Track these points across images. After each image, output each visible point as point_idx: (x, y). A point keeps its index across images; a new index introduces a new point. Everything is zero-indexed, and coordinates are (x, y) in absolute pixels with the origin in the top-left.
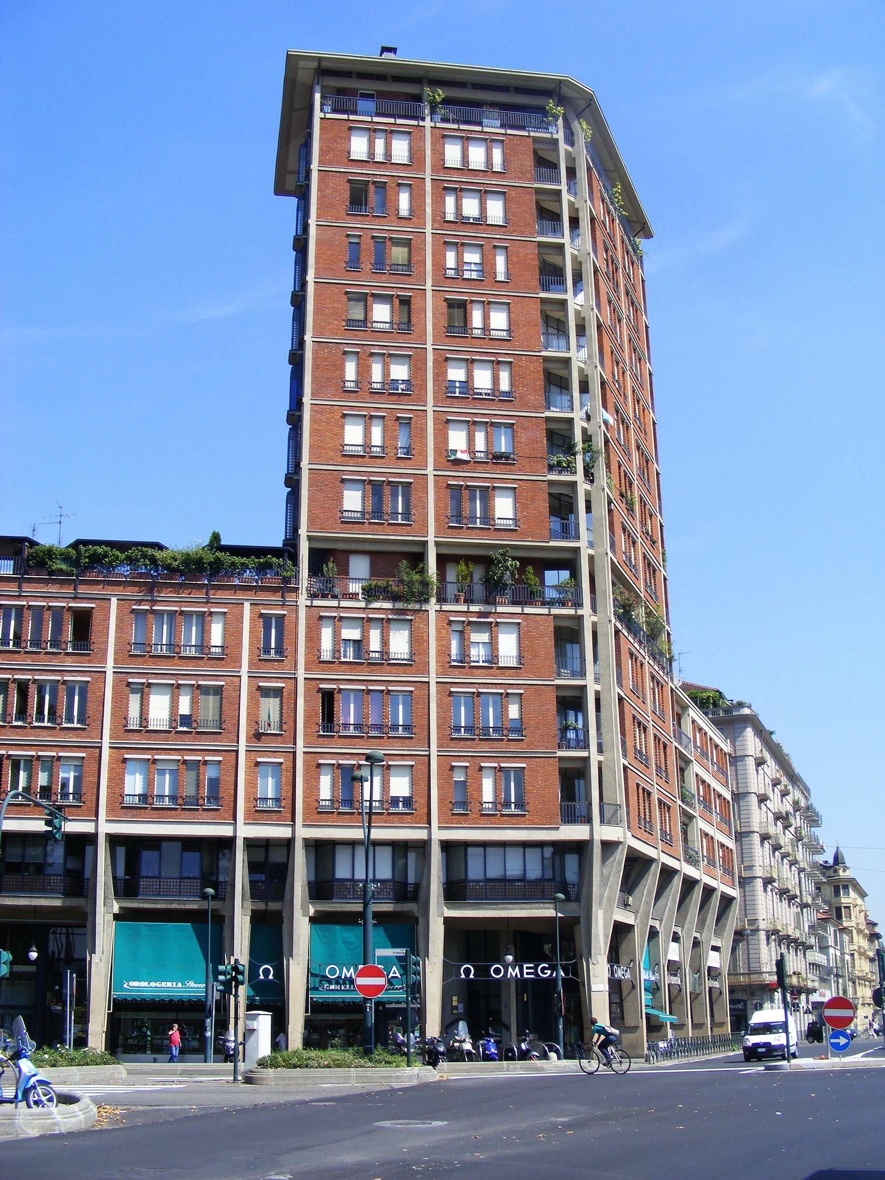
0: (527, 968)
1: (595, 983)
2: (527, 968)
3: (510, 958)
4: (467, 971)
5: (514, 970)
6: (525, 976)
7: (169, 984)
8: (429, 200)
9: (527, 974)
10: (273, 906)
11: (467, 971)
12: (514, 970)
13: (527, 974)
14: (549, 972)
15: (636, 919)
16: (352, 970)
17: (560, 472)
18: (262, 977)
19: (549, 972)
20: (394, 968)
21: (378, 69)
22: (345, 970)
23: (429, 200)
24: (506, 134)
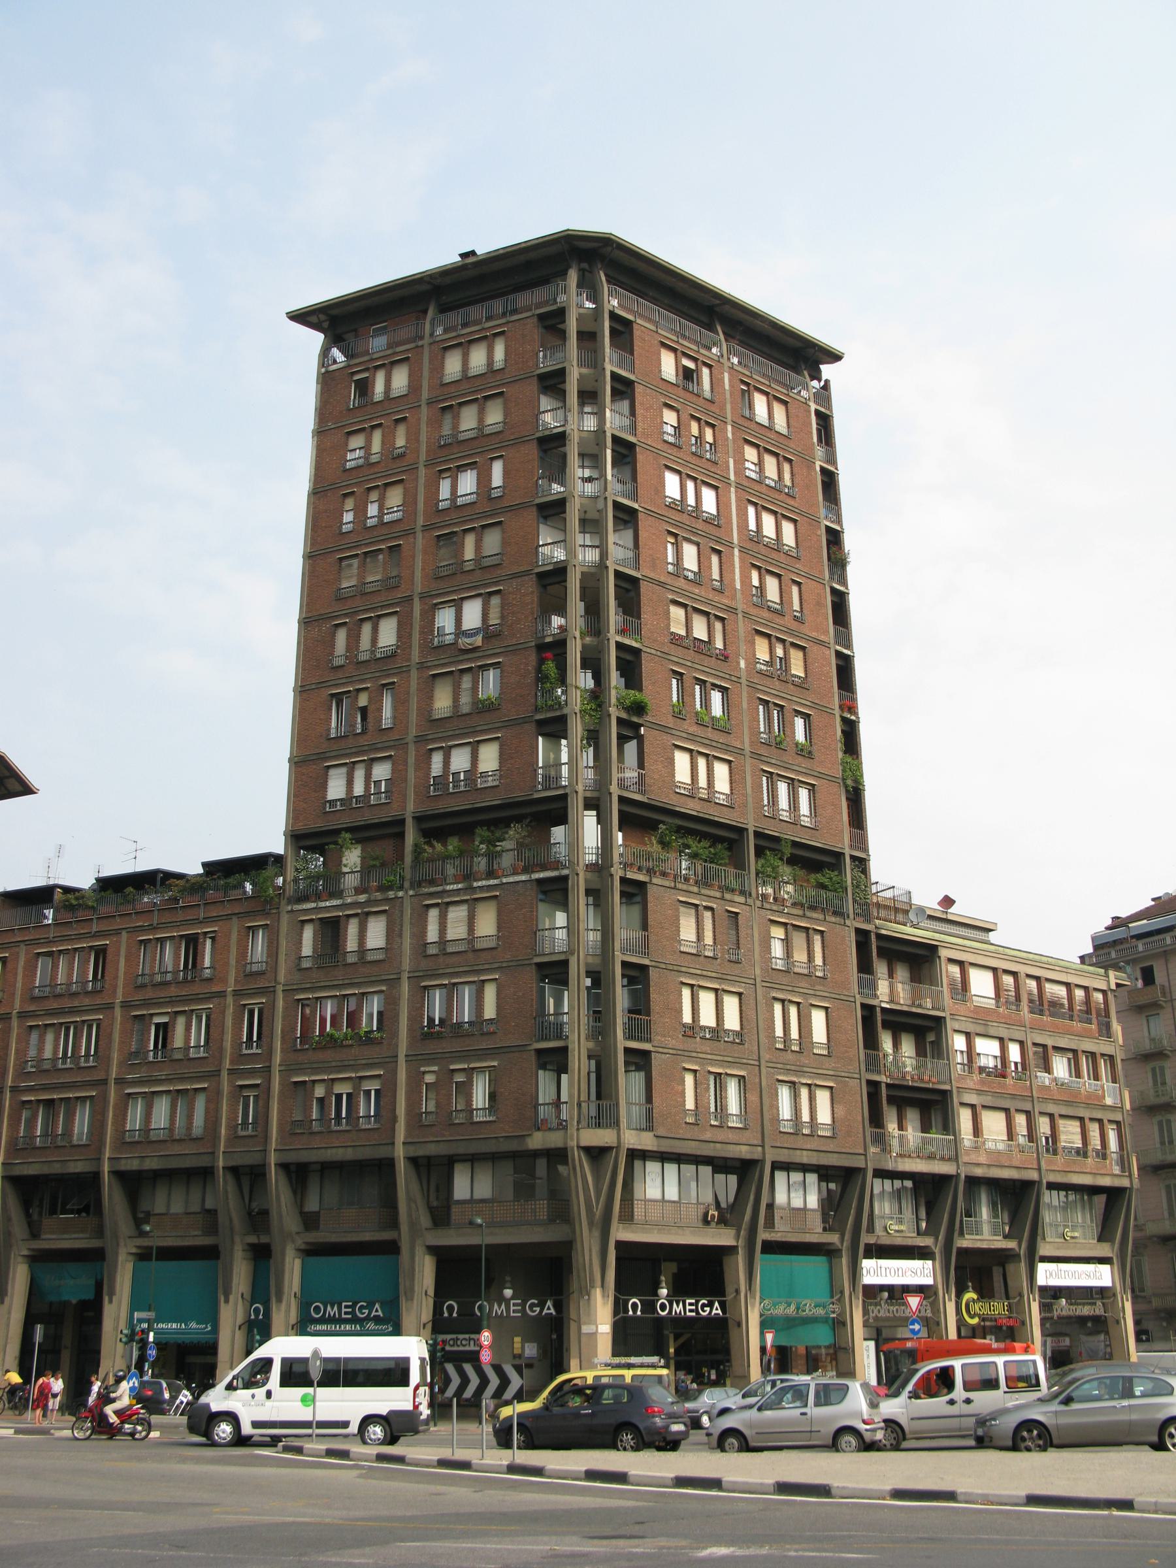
0: (346, 1307)
1: (585, 1323)
2: (346, 1307)
3: (508, 1293)
4: (450, 1308)
5: (500, 1307)
6: (688, 1314)
7: (174, 1326)
8: (737, 571)
9: (346, 1313)
10: (264, 1239)
11: (450, 1308)
12: (500, 1307)
13: (346, 1313)
14: (538, 1309)
15: (737, 1237)
16: (503, 1306)
17: (421, 633)
18: (446, 1315)
19: (538, 1309)
20: (377, 1306)
21: (357, 304)
22: (496, 1306)
23: (737, 571)
24: (508, 322)
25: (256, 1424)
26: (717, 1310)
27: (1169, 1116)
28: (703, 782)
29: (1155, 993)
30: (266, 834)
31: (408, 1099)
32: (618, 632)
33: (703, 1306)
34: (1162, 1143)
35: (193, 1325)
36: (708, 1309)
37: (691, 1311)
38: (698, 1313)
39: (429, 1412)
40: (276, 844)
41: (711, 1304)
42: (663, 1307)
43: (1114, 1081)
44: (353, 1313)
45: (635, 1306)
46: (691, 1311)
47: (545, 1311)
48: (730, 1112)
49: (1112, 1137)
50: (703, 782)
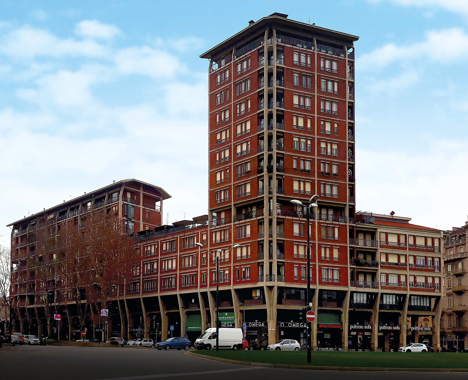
0: (297, 324)
5: (294, 325)
25: (422, 346)
26: (263, 325)
27: (461, 277)
28: (302, 189)
29: (185, 213)
30: (204, 211)
31: (233, 275)
32: (277, 149)
33: (260, 324)
34: (459, 285)
35: (198, 327)
36: (229, 325)
37: (257, 325)
38: (300, 326)
39: (424, 345)
40: (206, 213)
41: (261, 324)
42: (290, 325)
43: (438, 269)
44: (226, 326)
45: (282, 324)
46: (257, 325)
47: (304, 326)
48: (302, 276)
49: (296, 274)
50: (302, 189)
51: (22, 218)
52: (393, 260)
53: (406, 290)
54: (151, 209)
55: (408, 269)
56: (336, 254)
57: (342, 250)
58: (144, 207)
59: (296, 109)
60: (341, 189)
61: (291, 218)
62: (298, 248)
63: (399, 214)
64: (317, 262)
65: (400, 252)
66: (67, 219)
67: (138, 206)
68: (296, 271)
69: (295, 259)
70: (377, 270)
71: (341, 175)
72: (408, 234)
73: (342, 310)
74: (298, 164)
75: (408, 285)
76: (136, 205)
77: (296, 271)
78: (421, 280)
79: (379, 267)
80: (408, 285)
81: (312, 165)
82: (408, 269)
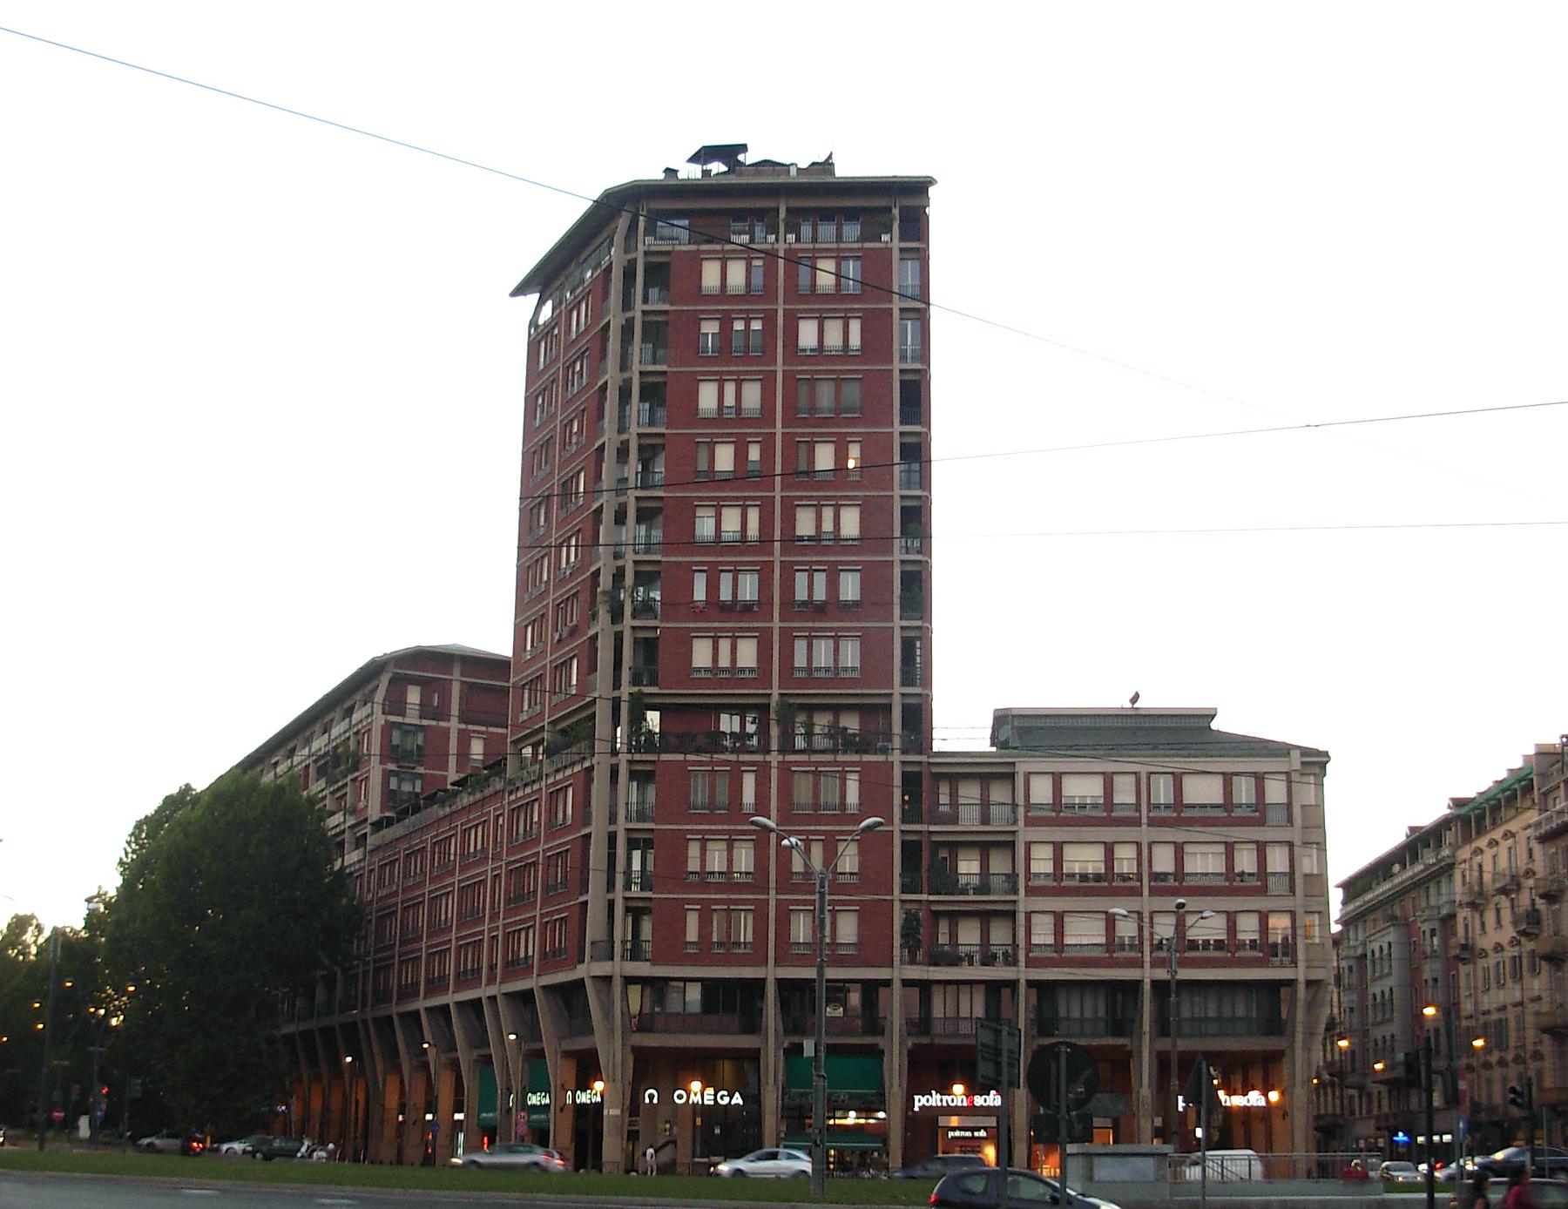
45: (651, 1097)
49: (692, 934)
51: (1117, 700)
52: (1084, 859)
53: (1139, 964)
54: (491, 729)
55: (1146, 891)
56: (849, 860)
57: (871, 842)
58: (463, 726)
59: (708, 422)
60: (874, 647)
61: (680, 757)
62: (703, 850)
63: (1161, 697)
64: (772, 892)
65: (1108, 834)
66: (501, 923)
67: (442, 724)
68: (692, 921)
69: (692, 888)
70: (1015, 902)
71: (874, 600)
72: (1144, 770)
73: (881, 1046)
74: (713, 587)
75: (1147, 949)
76: (434, 723)
77: (692, 921)
78: (1248, 928)
79: (1022, 891)
80: (1147, 949)
81: (765, 585)
82: (1146, 891)
